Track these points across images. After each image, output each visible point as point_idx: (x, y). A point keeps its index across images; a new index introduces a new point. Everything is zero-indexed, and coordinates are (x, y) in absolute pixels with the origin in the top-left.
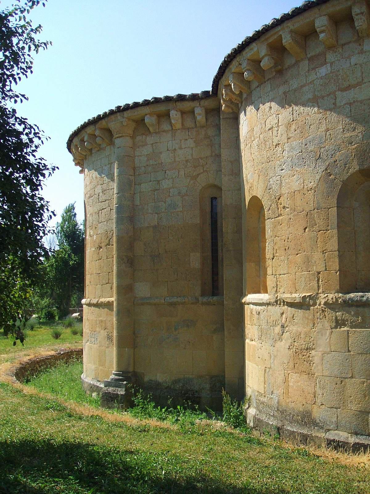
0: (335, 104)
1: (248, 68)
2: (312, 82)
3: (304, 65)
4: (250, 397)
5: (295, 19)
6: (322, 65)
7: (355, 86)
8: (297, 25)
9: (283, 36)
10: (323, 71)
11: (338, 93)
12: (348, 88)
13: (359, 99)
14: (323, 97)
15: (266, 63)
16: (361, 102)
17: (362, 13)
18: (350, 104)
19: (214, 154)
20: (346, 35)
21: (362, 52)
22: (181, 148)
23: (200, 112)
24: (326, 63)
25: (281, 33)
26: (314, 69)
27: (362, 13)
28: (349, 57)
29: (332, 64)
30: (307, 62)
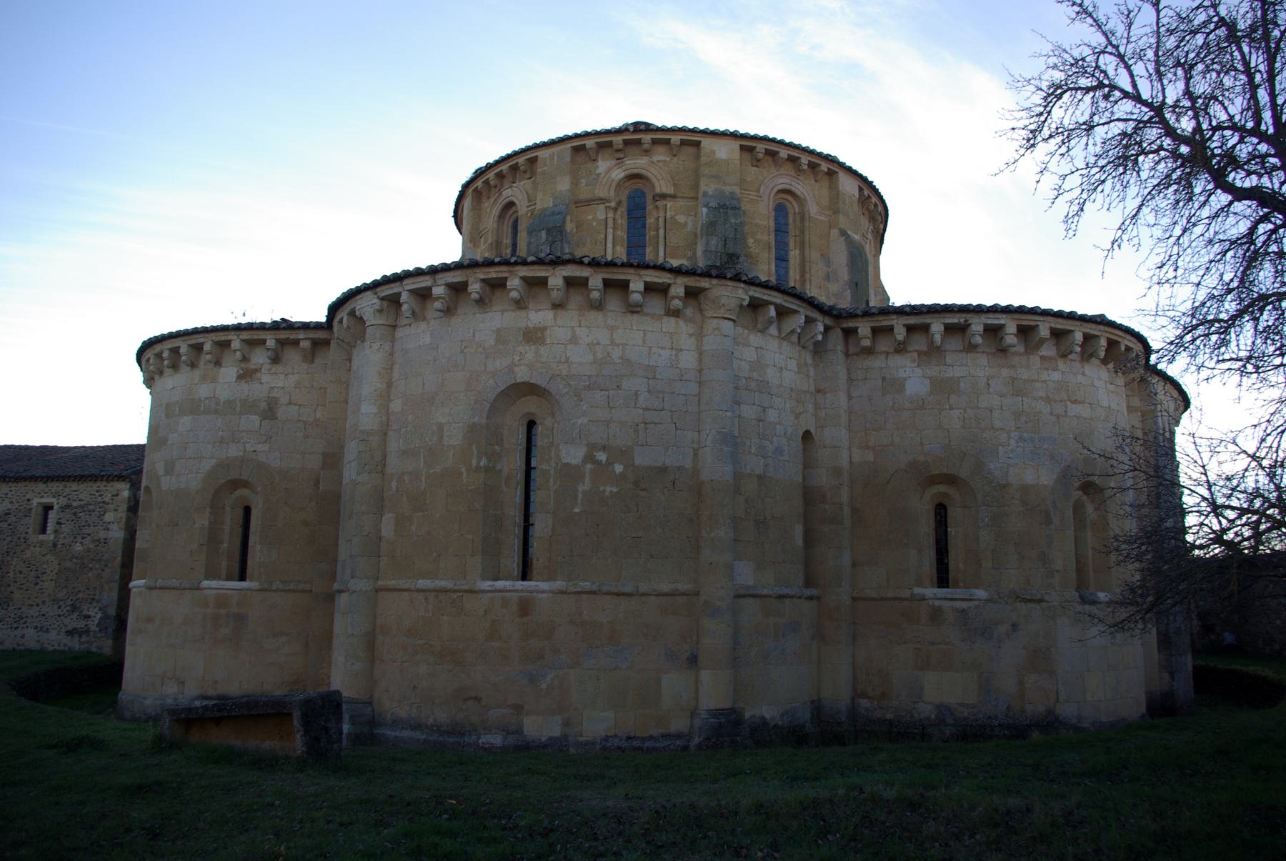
2: (1045, 381)
10: (1056, 376)
26: (1047, 369)
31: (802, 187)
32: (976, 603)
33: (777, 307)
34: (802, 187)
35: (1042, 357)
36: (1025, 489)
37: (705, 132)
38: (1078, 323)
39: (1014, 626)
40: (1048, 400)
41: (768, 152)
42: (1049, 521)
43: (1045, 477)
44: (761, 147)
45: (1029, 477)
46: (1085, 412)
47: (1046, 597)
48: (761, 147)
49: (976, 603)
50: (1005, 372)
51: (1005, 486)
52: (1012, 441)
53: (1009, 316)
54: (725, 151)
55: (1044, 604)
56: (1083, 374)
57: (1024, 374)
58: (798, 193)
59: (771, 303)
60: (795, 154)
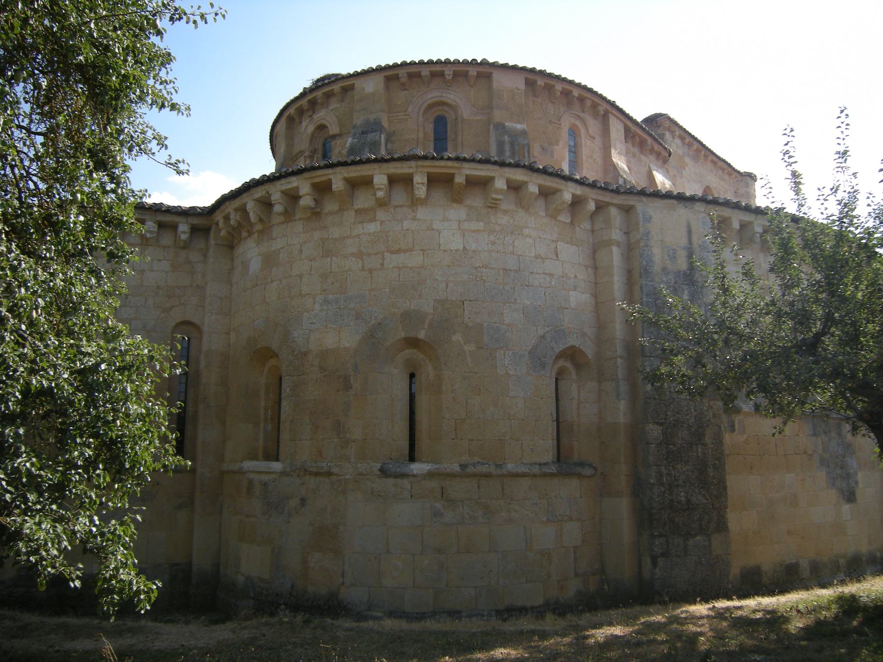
0: (382, 264)
1: (280, 201)
2: (358, 236)
3: (350, 216)
4: (690, 256)
5: (352, 168)
6: (371, 221)
7: (405, 251)
8: (352, 175)
9: (334, 181)
10: (372, 227)
11: (387, 255)
12: (398, 251)
13: (409, 265)
14: (369, 255)
15: (306, 201)
16: (411, 268)
17: (423, 183)
18: (399, 268)
19: (194, 285)
20: (399, 196)
21: (414, 219)
22: (152, 271)
23: (184, 228)
24: (375, 220)
25: (331, 177)
26: (362, 222)
27: (423, 183)
28: (401, 221)
29: (382, 222)
30: (353, 213)
31: (453, 96)
32: (274, 476)
33: (596, 201)
34: (453, 96)
35: (358, 211)
36: (324, 354)
37: (357, 75)
38: (375, 166)
39: (303, 500)
40: (360, 255)
41: (411, 76)
42: (348, 386)
43: (345, 338)
44: (402, 72)
45: (330, 341)
46: (414, 260)
47: (335, 470)
48: (402, 72)
49: (274, 476)
50: (317, 235)
51: (305, 354)
52: (317, 306)
53: (299, 177)
54: (370, 86)
55: (334, 478)
56: (414, 219)
57: (335, 232)
58: (449, 101)
59: (612, 204)
60: (438, 68)
